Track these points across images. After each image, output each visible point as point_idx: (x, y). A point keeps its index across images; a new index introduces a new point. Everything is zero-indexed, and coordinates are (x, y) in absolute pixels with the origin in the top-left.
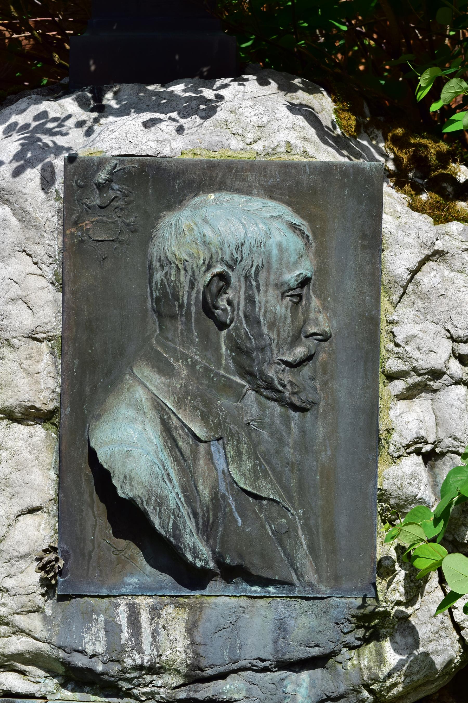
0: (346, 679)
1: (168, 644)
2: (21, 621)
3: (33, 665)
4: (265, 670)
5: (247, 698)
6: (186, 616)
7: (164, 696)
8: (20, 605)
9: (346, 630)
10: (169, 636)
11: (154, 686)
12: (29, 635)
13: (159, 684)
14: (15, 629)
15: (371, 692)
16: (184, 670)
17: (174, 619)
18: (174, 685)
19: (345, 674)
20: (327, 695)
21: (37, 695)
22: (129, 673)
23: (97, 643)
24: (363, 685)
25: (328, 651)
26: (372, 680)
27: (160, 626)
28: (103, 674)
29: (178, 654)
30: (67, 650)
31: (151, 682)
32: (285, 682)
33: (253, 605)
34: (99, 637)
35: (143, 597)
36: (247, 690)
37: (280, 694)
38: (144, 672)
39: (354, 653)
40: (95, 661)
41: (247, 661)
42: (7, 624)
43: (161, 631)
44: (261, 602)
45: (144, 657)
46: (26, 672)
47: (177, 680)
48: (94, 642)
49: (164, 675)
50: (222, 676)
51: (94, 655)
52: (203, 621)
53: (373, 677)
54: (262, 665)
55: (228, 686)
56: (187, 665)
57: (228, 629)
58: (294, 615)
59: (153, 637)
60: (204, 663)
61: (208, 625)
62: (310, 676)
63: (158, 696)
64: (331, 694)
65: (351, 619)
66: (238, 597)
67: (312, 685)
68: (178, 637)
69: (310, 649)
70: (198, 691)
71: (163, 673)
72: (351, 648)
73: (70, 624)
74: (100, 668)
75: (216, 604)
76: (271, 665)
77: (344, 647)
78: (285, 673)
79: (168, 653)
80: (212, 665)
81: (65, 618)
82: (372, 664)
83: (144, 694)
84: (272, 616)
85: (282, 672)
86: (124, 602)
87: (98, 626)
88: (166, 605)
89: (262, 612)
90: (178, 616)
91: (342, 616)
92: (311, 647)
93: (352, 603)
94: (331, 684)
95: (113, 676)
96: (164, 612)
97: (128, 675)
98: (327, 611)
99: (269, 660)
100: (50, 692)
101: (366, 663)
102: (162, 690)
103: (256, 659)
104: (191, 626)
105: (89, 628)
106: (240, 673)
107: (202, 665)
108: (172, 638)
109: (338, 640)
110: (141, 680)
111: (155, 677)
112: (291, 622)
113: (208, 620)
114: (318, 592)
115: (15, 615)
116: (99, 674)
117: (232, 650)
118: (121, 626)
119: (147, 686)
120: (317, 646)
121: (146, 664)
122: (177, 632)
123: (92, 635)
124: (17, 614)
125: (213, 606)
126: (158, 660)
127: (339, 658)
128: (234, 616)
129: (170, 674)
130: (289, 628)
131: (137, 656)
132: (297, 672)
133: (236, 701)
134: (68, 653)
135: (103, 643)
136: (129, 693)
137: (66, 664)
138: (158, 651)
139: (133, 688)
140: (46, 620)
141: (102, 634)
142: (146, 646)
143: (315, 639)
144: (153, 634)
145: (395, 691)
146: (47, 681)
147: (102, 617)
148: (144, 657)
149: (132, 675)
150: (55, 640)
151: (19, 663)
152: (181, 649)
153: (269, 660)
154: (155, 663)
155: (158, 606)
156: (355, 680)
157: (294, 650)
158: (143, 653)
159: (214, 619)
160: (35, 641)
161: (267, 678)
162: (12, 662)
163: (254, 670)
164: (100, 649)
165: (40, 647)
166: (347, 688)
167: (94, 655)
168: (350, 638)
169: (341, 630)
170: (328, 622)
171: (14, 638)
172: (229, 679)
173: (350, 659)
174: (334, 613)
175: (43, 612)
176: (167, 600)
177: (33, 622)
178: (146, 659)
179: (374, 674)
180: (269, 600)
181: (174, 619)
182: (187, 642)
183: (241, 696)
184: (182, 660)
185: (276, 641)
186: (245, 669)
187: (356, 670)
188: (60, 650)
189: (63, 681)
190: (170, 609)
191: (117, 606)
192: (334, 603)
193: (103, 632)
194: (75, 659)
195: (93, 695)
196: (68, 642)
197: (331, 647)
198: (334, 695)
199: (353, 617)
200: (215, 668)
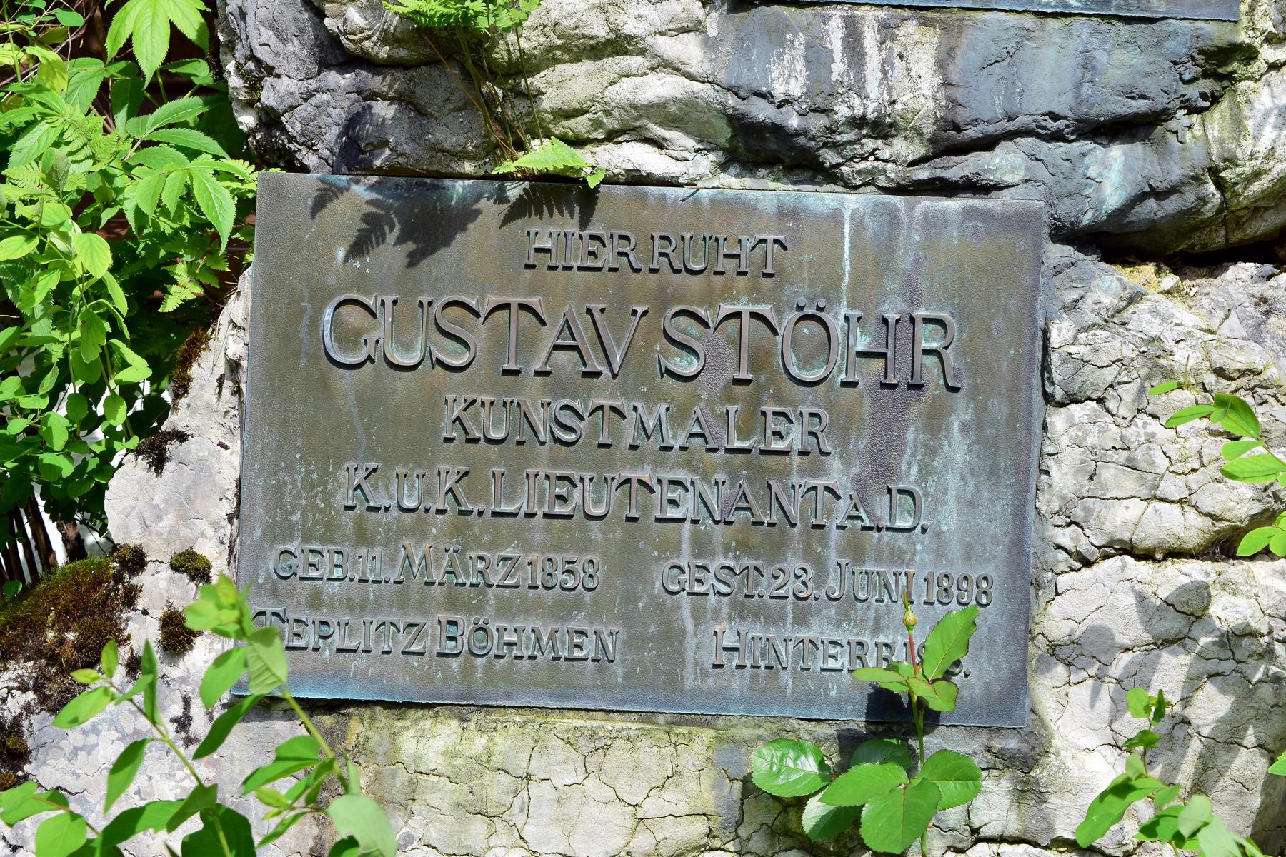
0: (1184, 158)
1: (907, 84)
2: (669, 47)
3: (677, 128)
4: (1057, 136)
5: (1026, 181)
6: (936, 40)
7: (893, 176)
8: (668, 18)
9: (1187, 77)
10: (909, 70)
11: (877, 159)
12: (677, 70)
13: (886, 156)
14: (655, 62)
15: (1220, 184)
16: (929, 128)
17: (916, 43)
18: (910, 158)
19: (1183, 149)
20: (1150, 186)
21: (681, 181)
22: (840, 133)
23: (792, 81)
24: (1210, 169)
25: (1159, 107)
26: (1225, 160)
27: (895, 55)
28: (798, 133)
29: (922, 99)
30: (742, 93)
31: (872, 153)
32: (1087, 160)
33: (1042, 28)
34: (795, 70)
35: (867, 8)
36: (1027, 169)
37: (1078, 179)
38: (864, 132)
39: (1195, 118)
40: (787, 112)
41: (1032, 118)
42: (643, 52)
43: (897, 62)
44: (1053, 24)
45: (868, 102)
46: (665, 139)
47: (917, 149)
48: (788, 78)
49: (895, 141)
50: (987, 144)
51: (787, 102)
52: (963, 48)
53: (1226, 155)
54: (1053, 125)
55: (997, 160)
56: (936, 120)
57: (1004, 64)
58: (1108, 46)
59: (884, 72)
60: (962, 116)
61: (971, 54)
62: (1125, 154)
63: (883, 178)
64: (1158, 184)
65: (1197, 56)
66: (1019, 12)
67: (1128, 168)
68: (921, 72)
69: (1132, 102)
70: (949, 168)
71: (893, 136)
72: (1193, 110)
73: (748, 49)
74: (794, 122)
75: (985, 22)
76: (1067, 126)
77: (1181, 108)
78: (1085, 145)
79: (905, 98)
80: (976, 120)
81: (740, 39)
82: (1225, 135)
83: (859, 172)
84: (1073, 45)
85: (1082, 142)
86: (839, 13)
87: (794, 53)
88: (905, 20)
89: (1057, 39)
90: (924, 40)
91: (1185, 50)
92: (1133, 98)
93: (1200, 29)
94: (1158, 168)
95: (813, 139)
96: (901, 32)
97: (838, 138)
98: (1159, 43)
99: (1065, 118)
100: (702, 176)
101: (1216, 134)
102: (890, 166)
103: (1044, 115)
104: (945, 56)
105: (780, 57)
106: (1017, 140)
107: (959, 120)
108: (913, 73)
109: (1175, 91)
110: (857, 146)
111: (880, 143)
112: (1101, 57)
113: (972, 47)
114: (1147, 10)
115: (658, 36)
116: (792, 136)
117: (1008, 97)
118: (832, 51)
119: (866, 159)
120: (1143, 97)
121: (871, 116)
122: (921, 64)
123: (784, 67)
124: (661, 34)
125: (980, 25)
126: (889, 110)
127: (1172, 125)
128: (1013, 41)
129: (906, 138)
130: (1099, 67)
131: (856, 102)
132: (1104, 146)
133: (1008, 186)
134: (744, 99)
135: (802, 80)
136: (834, 174)
137: (739, 122)
138: (890, 94)
139: (843, 164)
140: (710, 44)
141: (800, 66)
142: (873, 87)
143: (1140, 85)
144: (883, 66)
145: (1256, 187)
146: (698, 157)
147: (801, 37)
148: (868, 102)
149: (846, 137)
150: (722, 77)
151: (655, 123)
152: (928, 93)
153: (1065, 118)
154: (885, 116)
155: (892, 22)
156: (1197, 159)
157: (1106, 101)
158: (867, 97)
159: (981, 45)
160: (687, 81)
161: (1059, 151)
162: (646, 121)
163: (1039, 136)
164: (796, 89)
165: (695, 89)
166: (1185, 172)
167: (787, 102)
168: (1192, 92)
169: (1180, 74)
170: (1160, 59)
171: (652, 77)
172: (998, 150)
173: (1189, 127)
174: (1171, 45)
175: (703, 32)
176: (907, 13)
177: (687, 49)
178: (871, 106)
179: (1229, 150)
180: (1067, 21)
181: (916, 43)
182: (937, 81)
183: (1016, 179)
184: (929, 110)
185: (1078, 86)
186: (1024, 132)
187: (1200, 143)
188: (729, 94)
189: (723, 160)
190: (912, 26)
191: (826, 20)
192: (1171, 29)
193: (802, 62)
194: (753, 108)
195: (773, 180)
196: (748, 79)
197: (1161, 102)
198: (1162, 186)
199: (1200, 52)
200: (981, 127)
